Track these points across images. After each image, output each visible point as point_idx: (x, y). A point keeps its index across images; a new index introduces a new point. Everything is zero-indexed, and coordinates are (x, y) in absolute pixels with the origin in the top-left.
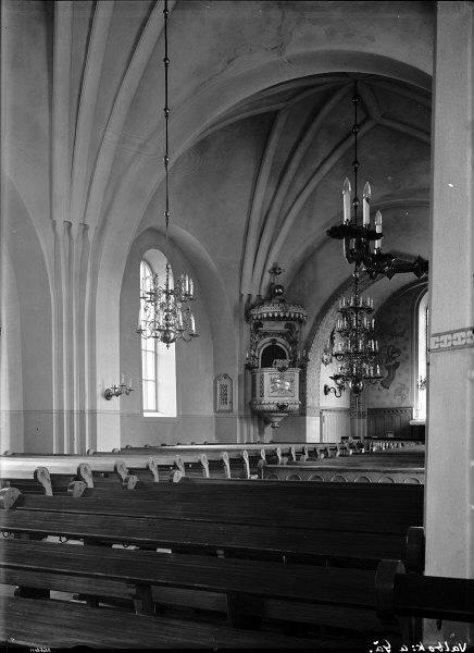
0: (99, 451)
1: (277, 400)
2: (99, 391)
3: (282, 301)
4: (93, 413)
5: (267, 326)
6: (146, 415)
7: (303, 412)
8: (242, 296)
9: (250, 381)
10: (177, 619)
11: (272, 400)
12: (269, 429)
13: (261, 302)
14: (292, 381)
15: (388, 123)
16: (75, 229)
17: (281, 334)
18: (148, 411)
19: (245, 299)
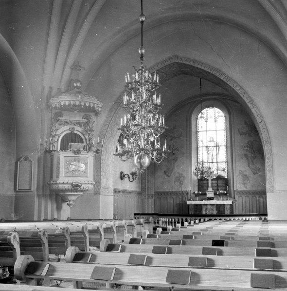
1: (71, 180)
7: (97, 193)
11: (66, 180)
12: (65, 206)
13: (60, 92)
14: (86, 164)
17: (79, 124)
19: (46, 91)
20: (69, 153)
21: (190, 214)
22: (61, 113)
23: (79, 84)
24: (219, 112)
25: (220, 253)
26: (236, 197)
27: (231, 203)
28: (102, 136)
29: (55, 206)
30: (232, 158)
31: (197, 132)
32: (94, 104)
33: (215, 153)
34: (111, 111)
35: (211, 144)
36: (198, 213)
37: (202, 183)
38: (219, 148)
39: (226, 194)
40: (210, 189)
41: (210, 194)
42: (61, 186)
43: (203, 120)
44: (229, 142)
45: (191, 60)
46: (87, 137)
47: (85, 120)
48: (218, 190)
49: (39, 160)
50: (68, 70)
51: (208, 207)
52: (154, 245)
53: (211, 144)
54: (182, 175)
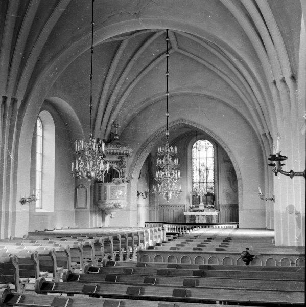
0: (16, 237)
2: (18, 199)
4: (14, 213)
6: (37, 211)
9: (97, 189)
10: (66, 100)
12: (107, 218)
14: (123, 191)
15: (181, 52)
16: (9, 102)
17: (116, 162)
18: (38, 208)
20: (112, 184)
21: (187, 222)
23: (117, 137)
24: (209, 144)
25: (211, 241)
26: (221, 209)
27: (217, 214)
28: (131, 171)
29: (101, 219)
30: (218, 180)
31: (192, 158)
33: (205, 176)
34: (137, 153)
35: (203, 168)
36: (194, 225)
37: (195, 199)
39: (213, 208)
40: (202, 203)
42: (107, 205)
44: (216, 155)
45: (192, 122)
46: (121, 171)
48: (207, 204)
49: (91, 187)
53: (203, 168)
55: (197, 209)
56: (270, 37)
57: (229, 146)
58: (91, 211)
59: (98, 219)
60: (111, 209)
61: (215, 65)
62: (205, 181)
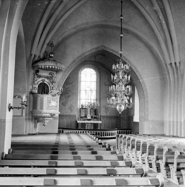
3: (55, 61)
5: (42, 73)
8: (31, 55)
19: (33, 56)
22: (38, 70)
24: (93, 72)
32: (62, 68)
33: (90, 94)
35: (88, 89)
38: (92, 92)
41: (89, 118)
43: (118, 85)
45: (112, 50)
47: (50, 76)
50: (45, 46)
51: (89, 124)
52: (53, 151)
54: (72, 105)
55: (86, 119)
56: (40, 35)
57: (140, 71)
58: (26, 119)
59: (32, 125)
60: (46, 117)
61: (142, 4)
62: (89, 98)
